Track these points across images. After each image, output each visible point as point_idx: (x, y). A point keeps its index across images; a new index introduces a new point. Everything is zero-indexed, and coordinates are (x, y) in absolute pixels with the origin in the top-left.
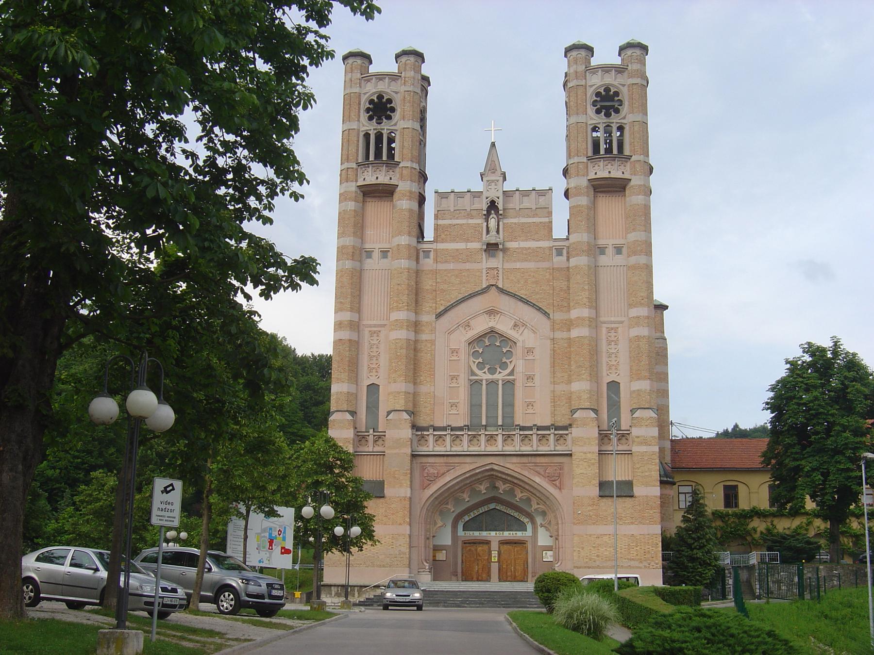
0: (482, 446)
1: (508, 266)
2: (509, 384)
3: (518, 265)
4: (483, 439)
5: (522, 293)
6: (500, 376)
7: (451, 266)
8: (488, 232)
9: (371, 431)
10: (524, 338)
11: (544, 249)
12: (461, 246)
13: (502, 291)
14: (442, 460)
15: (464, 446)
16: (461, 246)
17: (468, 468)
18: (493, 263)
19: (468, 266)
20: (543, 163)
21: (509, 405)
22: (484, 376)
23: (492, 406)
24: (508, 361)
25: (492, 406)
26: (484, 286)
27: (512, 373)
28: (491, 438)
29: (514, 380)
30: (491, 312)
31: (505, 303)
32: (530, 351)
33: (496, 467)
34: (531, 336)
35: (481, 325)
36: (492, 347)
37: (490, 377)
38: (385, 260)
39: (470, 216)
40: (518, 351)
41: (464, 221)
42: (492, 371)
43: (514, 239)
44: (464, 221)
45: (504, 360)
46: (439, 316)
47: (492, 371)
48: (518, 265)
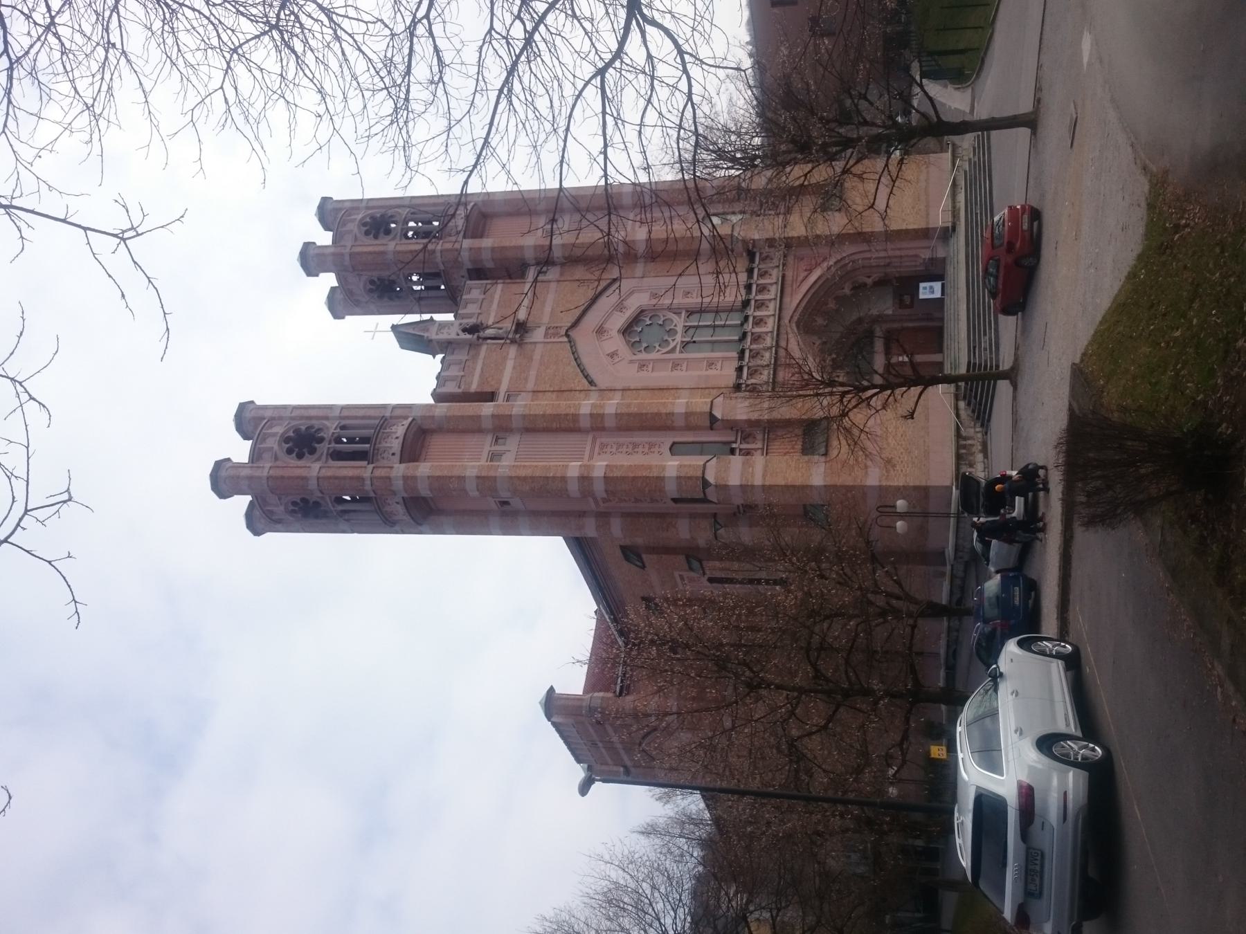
12: (510, 364)
13: (575, 324)
16: (510, 364)
18: (538, 335)
30: (600, 331)
33: (796, 318)
35: (615, 342)
42: (672, 332)
46: (591, 383)
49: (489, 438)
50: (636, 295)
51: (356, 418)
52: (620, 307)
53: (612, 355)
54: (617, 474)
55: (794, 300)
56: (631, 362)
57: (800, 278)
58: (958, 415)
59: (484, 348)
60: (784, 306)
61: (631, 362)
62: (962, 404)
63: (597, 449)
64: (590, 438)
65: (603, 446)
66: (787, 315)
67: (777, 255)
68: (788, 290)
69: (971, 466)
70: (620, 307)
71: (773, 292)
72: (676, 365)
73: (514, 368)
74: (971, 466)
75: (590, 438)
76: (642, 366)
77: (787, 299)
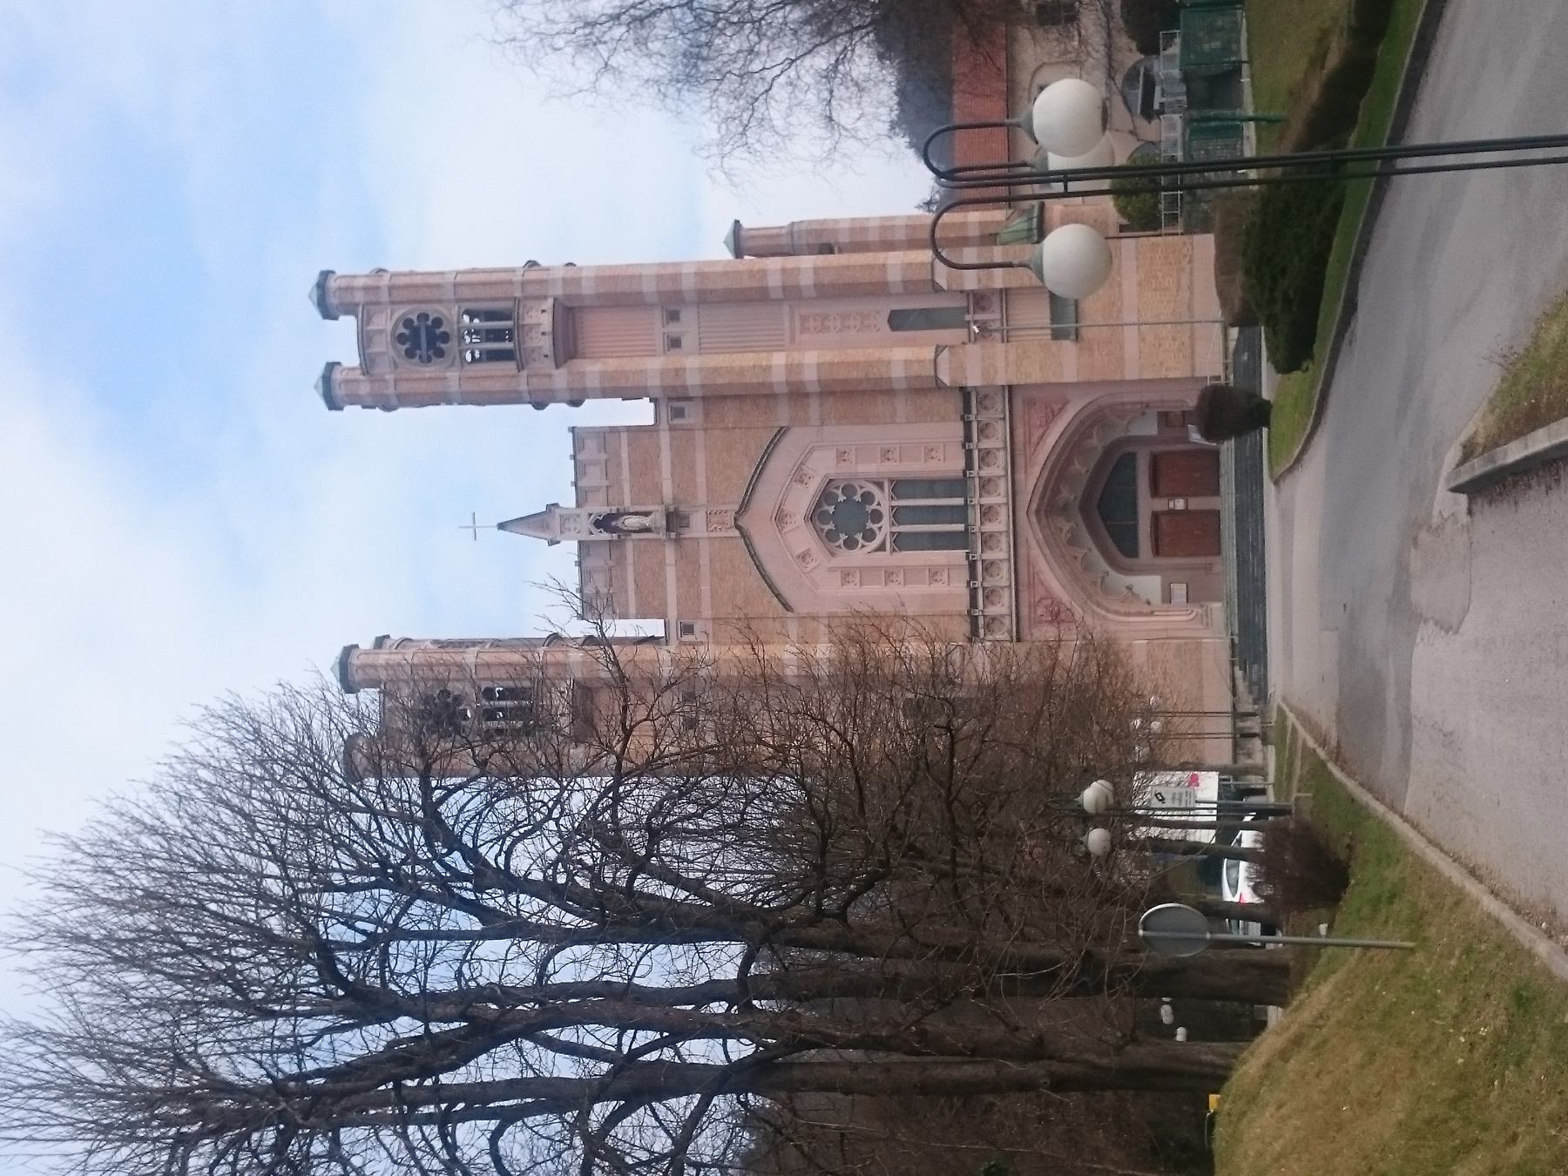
0: (1000, 525)
1: (702, 497)
2: (900, 486)
3: (701, 480)
4: (989, 527)
5: (748, 472)
6: (884, 501)
7: (705, 588)
8: (647, 530)
9: (968, 317)
10: (823, 466)
11: (672, 438)
12: (671, 574)
13: (744, 506)
14: (1024, 595)
15: (1000, 553)
16: (671, 574)
17: (1036, 552)
19: (704, 561)
20: (524, 450)
21: (931, 486)
22: (885, 529)
23: (935, 514)
24: (860, 492)
25: (935, 514)
26: (737, 533)
27: (880, 485)
28: (987, 513)
29: (891, 481)
30: (780, 518)
31: (765, 500)
32: (841, 456)
33: (1034, 506)
34: (820, 455)
35: (802, 537)
36: (841, 515)
37: (886, 522)
38: (683, 315)
39: (621, 561)
40: (845, 469)
41: (630, 569)
42: (877, 516)
43: (658, 488)
44: (630, 569)
45: (858, 498)
46: (787, 606)
47: (877, 516)
48: (701, 480)
49: (657, 316)
50: (816, 455)
51: (485, 300)
52: (800, 477)
53: (804, 557)
54: (827, 279)
55: (1031, 479)
56: (832, 570)
57: (1035, 439)
58: (1234, 694)
59: (629, 546)
60: (1018, 488)
61: (832, 570)
62: (1239, 673)
63: (797, 324)
64: (786, 309)
65: (804, 319)
66: (1024, 500)
67: (999, 406)
68: (1020, 461)
69: (1249, 755)
70: (800, 477)
71: (1002, 458)
72: (889, 574)
73: (678, 580)
74: (1249, 755)
75: (786, 309)
76: (846, 575)
77: (1020, 476)
